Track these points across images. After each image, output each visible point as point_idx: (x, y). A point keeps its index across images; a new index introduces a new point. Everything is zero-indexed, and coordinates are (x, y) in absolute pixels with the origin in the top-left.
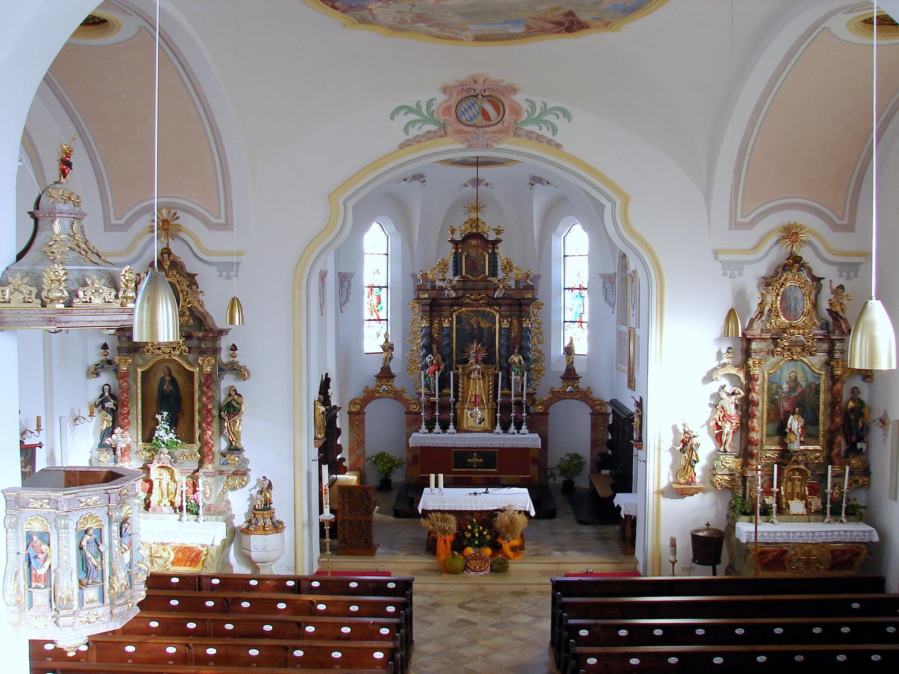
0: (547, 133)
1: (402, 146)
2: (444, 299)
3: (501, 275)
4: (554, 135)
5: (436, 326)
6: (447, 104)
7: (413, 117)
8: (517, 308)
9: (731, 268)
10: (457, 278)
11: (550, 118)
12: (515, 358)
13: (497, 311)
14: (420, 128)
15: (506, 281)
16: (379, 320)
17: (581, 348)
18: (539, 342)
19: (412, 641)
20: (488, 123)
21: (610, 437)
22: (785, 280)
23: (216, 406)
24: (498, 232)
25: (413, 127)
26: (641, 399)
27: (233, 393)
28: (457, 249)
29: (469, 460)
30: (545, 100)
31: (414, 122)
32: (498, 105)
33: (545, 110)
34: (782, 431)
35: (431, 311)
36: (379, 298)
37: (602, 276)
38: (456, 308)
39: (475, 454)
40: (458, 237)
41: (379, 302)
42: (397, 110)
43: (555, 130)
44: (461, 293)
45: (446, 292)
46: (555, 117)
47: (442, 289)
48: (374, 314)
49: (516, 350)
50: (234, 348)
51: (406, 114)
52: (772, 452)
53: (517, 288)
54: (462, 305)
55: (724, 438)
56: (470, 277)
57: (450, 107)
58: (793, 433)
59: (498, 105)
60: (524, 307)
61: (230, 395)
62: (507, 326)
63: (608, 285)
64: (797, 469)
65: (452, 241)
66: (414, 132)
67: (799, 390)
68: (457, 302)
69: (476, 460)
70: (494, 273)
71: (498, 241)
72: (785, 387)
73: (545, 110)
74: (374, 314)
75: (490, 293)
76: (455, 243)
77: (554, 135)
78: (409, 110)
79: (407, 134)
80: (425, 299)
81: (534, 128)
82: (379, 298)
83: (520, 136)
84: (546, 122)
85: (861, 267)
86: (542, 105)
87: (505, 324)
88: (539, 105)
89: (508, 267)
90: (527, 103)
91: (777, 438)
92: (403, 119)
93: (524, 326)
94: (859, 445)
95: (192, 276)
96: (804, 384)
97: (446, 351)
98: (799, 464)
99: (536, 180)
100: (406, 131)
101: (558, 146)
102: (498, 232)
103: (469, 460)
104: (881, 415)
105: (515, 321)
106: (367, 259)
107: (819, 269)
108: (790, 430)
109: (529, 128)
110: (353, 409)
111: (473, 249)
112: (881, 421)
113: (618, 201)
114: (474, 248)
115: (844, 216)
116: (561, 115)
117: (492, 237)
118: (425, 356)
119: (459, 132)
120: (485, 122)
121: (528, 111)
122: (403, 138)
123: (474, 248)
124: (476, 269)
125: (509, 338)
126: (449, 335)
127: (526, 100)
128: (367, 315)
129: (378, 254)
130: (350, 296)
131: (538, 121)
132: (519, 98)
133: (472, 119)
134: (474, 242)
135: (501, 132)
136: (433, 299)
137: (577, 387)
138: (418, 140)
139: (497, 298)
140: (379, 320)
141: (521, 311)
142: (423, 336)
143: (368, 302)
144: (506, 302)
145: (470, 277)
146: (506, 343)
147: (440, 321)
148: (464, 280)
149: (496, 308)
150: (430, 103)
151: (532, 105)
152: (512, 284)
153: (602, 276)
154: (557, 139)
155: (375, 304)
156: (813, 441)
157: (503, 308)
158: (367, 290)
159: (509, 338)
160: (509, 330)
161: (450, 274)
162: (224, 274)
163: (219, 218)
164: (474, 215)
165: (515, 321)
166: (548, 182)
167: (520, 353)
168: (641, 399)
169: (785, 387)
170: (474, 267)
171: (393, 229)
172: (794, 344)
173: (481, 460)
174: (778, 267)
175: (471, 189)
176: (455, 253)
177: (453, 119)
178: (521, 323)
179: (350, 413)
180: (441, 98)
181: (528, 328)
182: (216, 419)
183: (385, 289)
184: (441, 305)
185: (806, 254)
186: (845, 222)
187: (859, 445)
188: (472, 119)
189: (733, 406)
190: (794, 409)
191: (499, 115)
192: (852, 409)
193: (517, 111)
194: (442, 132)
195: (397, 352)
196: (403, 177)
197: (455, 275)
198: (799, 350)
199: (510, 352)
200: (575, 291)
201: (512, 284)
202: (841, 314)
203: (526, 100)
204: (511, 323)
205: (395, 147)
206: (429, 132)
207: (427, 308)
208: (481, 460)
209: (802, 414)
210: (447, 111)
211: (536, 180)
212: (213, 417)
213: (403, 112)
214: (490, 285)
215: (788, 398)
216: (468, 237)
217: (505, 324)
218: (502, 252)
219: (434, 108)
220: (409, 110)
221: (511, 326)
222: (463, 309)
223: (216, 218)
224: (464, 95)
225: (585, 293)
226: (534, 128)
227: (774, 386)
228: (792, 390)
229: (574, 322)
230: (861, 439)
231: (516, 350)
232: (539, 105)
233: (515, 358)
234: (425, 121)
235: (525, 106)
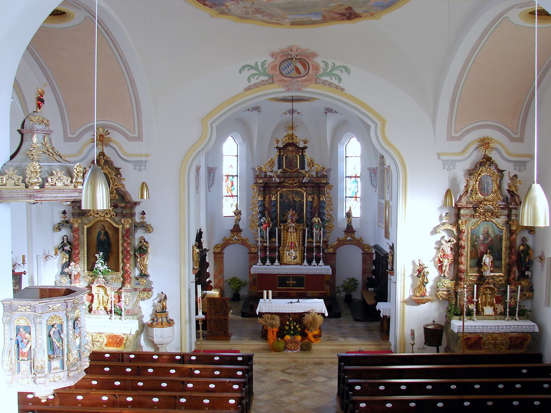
0: (335, 81)
1: (247, 90)
2: (272, 183)
3: (307, 168)
4: (339, 83)
5: (267, 200)
6: (274, 64)
7: (253, 71)
8: (317, 189)
9: (449, 164)
10: (280, 171)
11: (337, 72)
12: (316, 220)
13: (305, 191)
14: (257, 79)
15: (310, 172)
16: (232, 196)
17: (356, 213)
18: (330, 210)
19: (252, 393)
20: (299, 75)
21: (374, 268)
22: (481, 171)
23: (133, 249)
24: (305, 142)
25: (253, 78)
26: (393, 245)
27: (143, 241)
28: (280, 152)
29: (288, 282)
30: (334, 61)
31: (254, 75)
32: (305, 65)
33: (334, 68)
34: (479, 264)
35: (264, 191)
36: (232, 182)
37: (369, 169)
38: (279, 189)
39: (291, 278)
40: (281, 145)
41: (232, 185)
42: (244, 68)
43: (340, 80)
44: (282, 179)
45: (274, 179)
46: (340, 72)
47: (271, 177)
48: (229, 192)
49: (316, 215)
50: (143, 213)
51: (249, 70)
52: (473, 277)
53: (317, 177)
54: (283, 187)
55: (444, 268)
56: (288, 169)
57: (276, 65)
58: (486, 265)
59: (305, 65)
60: (321, 188)
61: (141, 242)
62: (311, 200)
63: (373, 175)
64: (489, 288)
65: (277, 148)
66: (254, 81)
67: (490, 239)
68: (280, 185)
69: (291, 282)
70: (303, 167)
71: (306, 148)
72: (481, 237)
73: (334, 68)
74: (229, 192)
75: (301, 180)
76: (279, 149)
77: (339, 83)
78: (251, 67)
79: (250, 82)
80: (261, 183)
81: (327, 79)
82: (232, 182)
83: (318, 83)
84: (335, 75)
85: (528, 163)
86: (332, 64)
87: (310, 199)
88: (330, 65)
89: (312, 163)
90: (323, 63)
91: (476, 269)
92: (247, 73)
93: (321, 199)
94: (527, 273)
95: (117, 169)
96: (493, 235)
97: (274, 215)
98: (489, 284)
99: (328, 110)
100: (249, 80)
101: (342, 89)
102: (305, 142)
103: (288, 282)
104: (540, 254)
105: (316, 197)
106: (225, 159)
107: (502, 165)
108: (484, 263)
109: (324, 78)
110: (216, 251)
111: (290, 152)
112: (540, 258)
113: (379, 123)
114: (291, 152)
115: (517, 132)
116: (344, 71)
117: (301, 145)
118: (261, 218)
119: (281, 81)
120: (297, 75)
121: (323, 68)
122: (247, 84)
123: (291, 152)
124: (291, 165)
125: (312, 207)
126: (276, 205)
127: (323, 61)
128: (225, 193)
129: (231, 156)
130: (215, 181)
131: (330, 74)
132: (318, 60)
133: (289, 73)
134: (290, 148)
135: (307, 81)
136: (266, 183)
137: (354, 237)
138: (256, 86)
139: (305, 183)
140: (232, 196)
141: (319, 190)
142: (259, 206)
143: (225, 185)
144: (310, 185)
145: (288, 169)
146: (310, 210)
147: (270, 196)
148: (285, 172)
149: (304, 189)
150: (263, 63)
151: (326, 64)
152: (314, 174)
153: (369, 169)
154: (341, 85)
155: (230, 187)
156: (498, 270)
157: (308, 189)
158: (225, 178)
159: (312, 207)
160: (312, 202)
161: (276, 168)
162: (138, 168)
163: (134, 133)
164: (290, 132)
165: (316, 197)
166: (336, 112)
167: (319, 216)
168: (393, 245)
169: (481, 237)
170: (290, 164)
171: (241, 140)
172: (487, 211)
173: (295, 282)
174: (477, 164)
175: (289, 116)
176: (279, 155)
177: (277, 73)
178: (319, 198)
179: (214, 253)
180: (270, 60)
181: (323, 201)
182: (133, 257)
183: (236, 177)
184: (270, 187)
185: (494, 156)
186: (518, 136)
187: (527, 273)
188: (289, 73)
189: (449, 249)
190: (487, 251)
191: (306, 70)
192: (522, 251)
193: (317, 68)
194: (271, 81)
195: (243, 216)
196: (247, 109)
197: (279, 168)
198: (490, 214)
199: (313, 216)
200: (352, 178)
201: (314, 174)
202: (515, 192)
203: (323, 61)
204: (313, 198)
205: (242, 90)
206: (263, 81)
207: (262, 189)
208: (295, 282)
209: (491, 253)
210: (274, 68)
211: (328, 110)
212: (131, 256)
213: (247, 69)
214: (301, 175)
215: (483, 244)
216: (287, 145)
217: (310, 199)
218: (308, 154)
219: (266, 66)
220: (251, 67)
221: (313, 200)
222: (284, 189)
223: (132, 134)
224: (285, 58)
225: (358, 179)
226: (327, 79)
227: (474, 237)
228: (485, 239)
229: (352, 197)
230: (528, 269)
231: (316, 215)
232: (330, 65)
233: (316, 220)
234: (260, 74)
235: (322, 65)
